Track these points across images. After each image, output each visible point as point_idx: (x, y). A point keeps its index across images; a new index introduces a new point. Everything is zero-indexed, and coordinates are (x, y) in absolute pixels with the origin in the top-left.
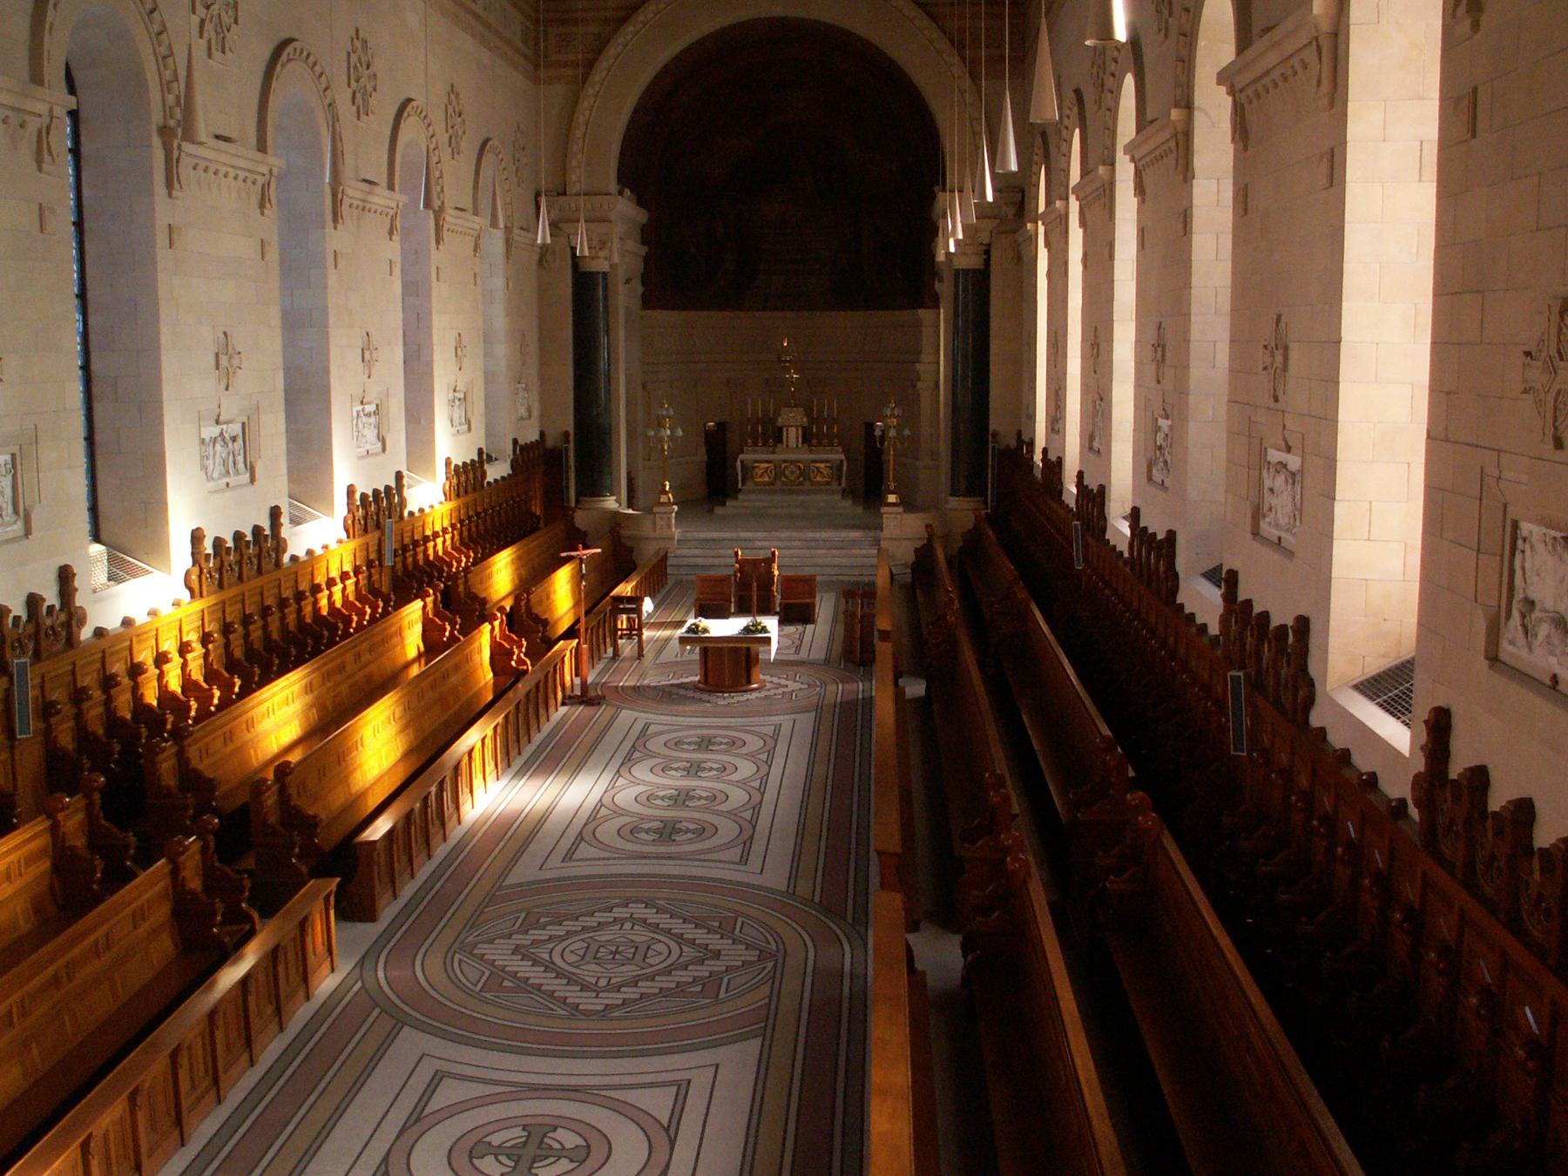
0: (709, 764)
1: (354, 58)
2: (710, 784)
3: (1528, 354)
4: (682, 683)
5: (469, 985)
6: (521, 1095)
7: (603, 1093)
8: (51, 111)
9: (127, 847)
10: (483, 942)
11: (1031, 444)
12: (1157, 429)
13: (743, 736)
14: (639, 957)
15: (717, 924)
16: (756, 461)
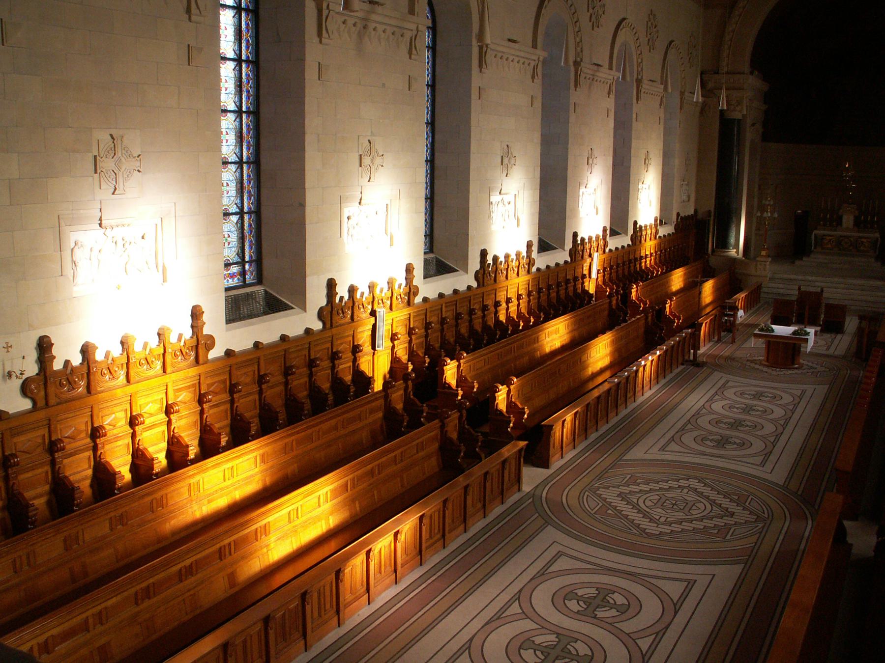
2: (755, 419)
5: (589, 509)
6: (601, 572)
7: (646, 579)
8: (417, 28)
9: (422, 412)
10: (602, 488)
13: (782, 394)
14: (687, 509)
15: (737, 497)
16: (824, 235)
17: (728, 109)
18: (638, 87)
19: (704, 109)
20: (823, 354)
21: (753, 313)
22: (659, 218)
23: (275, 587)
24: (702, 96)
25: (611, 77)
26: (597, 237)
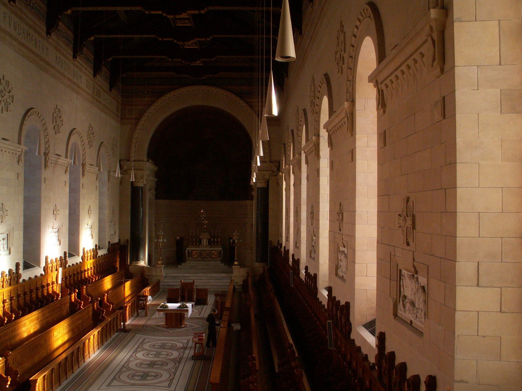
0: (163, 353)
1: (55, 115)
3: (400, 215)
4: (159, 325)
11: (281, 245)
12: (313, 240)
16: (193, 250)
17: (135, 181)
18: (83, 168)
19: (121, 182)
20: (197, 318)
21: (157, 297)
22: (98, 245)
23: (58, 355)
24: (121, 174)
25: (67, 163)
26: (61, 257)
